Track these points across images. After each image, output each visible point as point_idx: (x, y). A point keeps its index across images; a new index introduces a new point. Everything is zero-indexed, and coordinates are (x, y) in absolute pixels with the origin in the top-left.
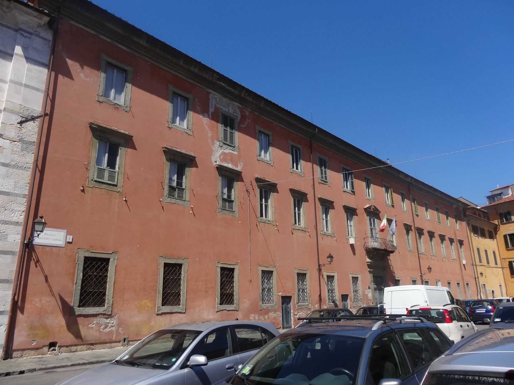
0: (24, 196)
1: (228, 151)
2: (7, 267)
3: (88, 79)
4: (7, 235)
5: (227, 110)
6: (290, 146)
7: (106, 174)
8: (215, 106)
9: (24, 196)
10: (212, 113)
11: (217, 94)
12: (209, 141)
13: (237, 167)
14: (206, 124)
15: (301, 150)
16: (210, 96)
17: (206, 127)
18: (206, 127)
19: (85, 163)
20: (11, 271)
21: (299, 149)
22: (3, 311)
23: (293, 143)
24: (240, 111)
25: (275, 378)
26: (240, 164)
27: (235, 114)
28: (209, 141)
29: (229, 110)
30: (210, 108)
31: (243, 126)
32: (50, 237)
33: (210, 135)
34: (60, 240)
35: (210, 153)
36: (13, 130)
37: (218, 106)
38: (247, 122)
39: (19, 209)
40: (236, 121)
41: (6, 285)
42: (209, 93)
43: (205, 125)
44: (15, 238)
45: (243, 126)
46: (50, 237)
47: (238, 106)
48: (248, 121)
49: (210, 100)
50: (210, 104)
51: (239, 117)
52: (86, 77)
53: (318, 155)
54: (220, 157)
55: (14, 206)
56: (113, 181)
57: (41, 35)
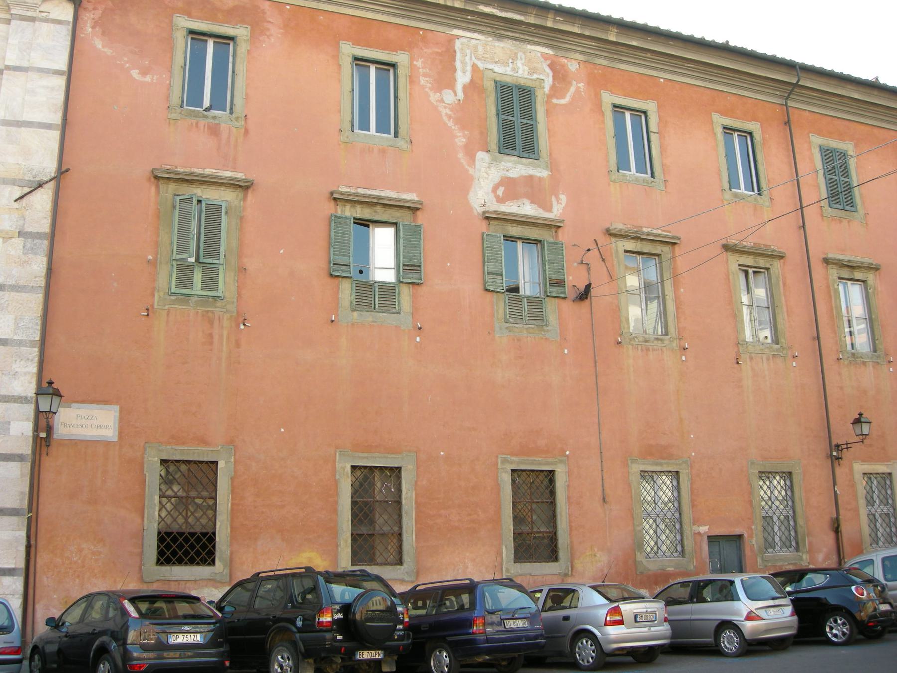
0: (32, 344)
1: (517, 168)
2: (5, 483)
3: (148, 79)
4: (9, 423)
5: (508, 70)
6: (719, 130)
7: (198, 276)
8: (475, 66)
9: (32, 344)
10: (465, 87)
11: (476, 36)
12: (461, 155)
13: (550, 210)
14: (450, 117)
15: (758, 136)
16: (458, 44)
17: (450, 123)
18: (450, 123)
19: (150, 257)
20: (22, 493)
21: (751, 134)
22: (14, 569)
23: (728, 122)
24: (551, 66)
25: (531, 178)
26: (558, 199)
27: (535, 76)
28: (461, 155)
29: (515, 70)
30: (459, 74)
31: (562, 101)
32: (87, 422)
33: (461, 140)
34: (107, 427)
35: (465, 184)
36: (7, 216)
37: (481, 65)
38: (572, 89)
39: (27, 370)
40: (539, 93)
41: (15, 520)
42: (452, 39)
43: (445, 118)
44: (21, 429)
45: (562, 101)
46: (87, 422)
47: (543, 54)
48: (577, 86)
49: (459, 56)
50: (458, 64)
51: (548, 82)
52: (144, 73)
53: (817, 140)
54: (495, 190)
55: (18, 367)
56: (211, 290)
57: (52, 16)
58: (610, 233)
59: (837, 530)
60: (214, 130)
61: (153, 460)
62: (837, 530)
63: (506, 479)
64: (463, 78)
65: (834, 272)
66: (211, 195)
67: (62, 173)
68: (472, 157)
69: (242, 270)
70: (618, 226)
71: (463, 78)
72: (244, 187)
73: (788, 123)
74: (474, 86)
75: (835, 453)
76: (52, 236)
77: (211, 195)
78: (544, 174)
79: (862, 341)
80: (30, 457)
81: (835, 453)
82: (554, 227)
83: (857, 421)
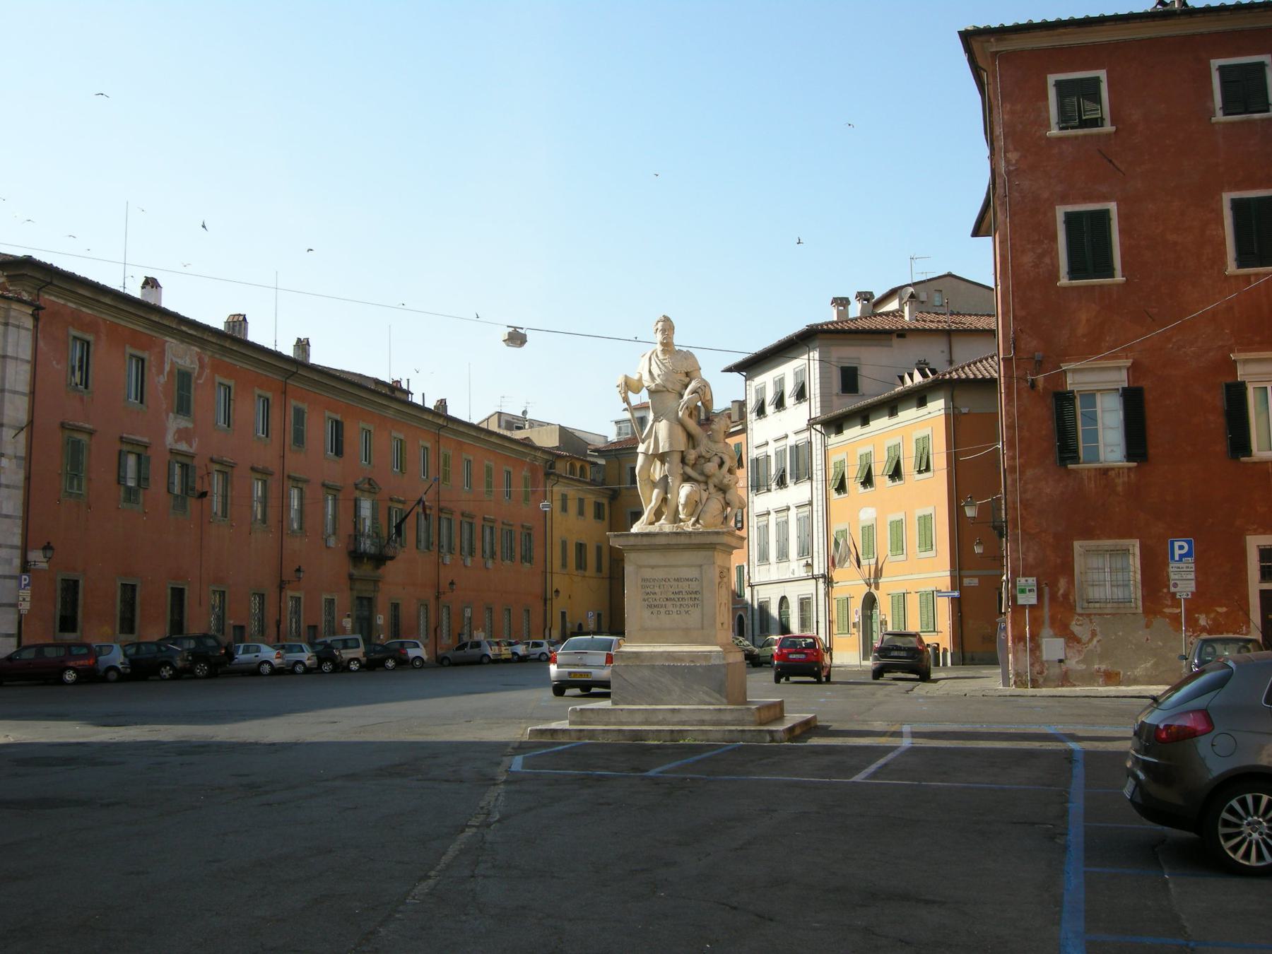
0: (28, 362)
1: (184, 423)
9: (28, 362)
58: (212, 460)
59: (278, 627)
60: (82, 400)
61: (59, 578)
62: (278, 627)
63: (169, 591)
64: (167, 368)
65: (291, 482)
66: (78, 436)
67: (31, 423)
68: (167, 415)
69: (90, 480)
70: (215, 457)
71: (167, 368)
72: (91, 433)
73: (285, 393)
74: (171, 372)
75: (281, 586)
76: (33, 393)
77: (78, 436)
78: (190, 426)
79: (295, 526)
80: (152, 301)
81: (281, 586)
82: (192, 457)
83: (298, 570)
